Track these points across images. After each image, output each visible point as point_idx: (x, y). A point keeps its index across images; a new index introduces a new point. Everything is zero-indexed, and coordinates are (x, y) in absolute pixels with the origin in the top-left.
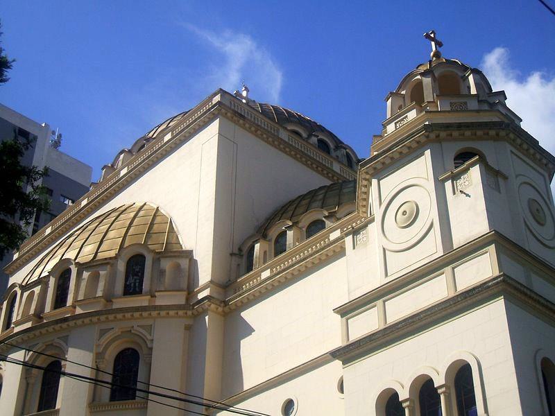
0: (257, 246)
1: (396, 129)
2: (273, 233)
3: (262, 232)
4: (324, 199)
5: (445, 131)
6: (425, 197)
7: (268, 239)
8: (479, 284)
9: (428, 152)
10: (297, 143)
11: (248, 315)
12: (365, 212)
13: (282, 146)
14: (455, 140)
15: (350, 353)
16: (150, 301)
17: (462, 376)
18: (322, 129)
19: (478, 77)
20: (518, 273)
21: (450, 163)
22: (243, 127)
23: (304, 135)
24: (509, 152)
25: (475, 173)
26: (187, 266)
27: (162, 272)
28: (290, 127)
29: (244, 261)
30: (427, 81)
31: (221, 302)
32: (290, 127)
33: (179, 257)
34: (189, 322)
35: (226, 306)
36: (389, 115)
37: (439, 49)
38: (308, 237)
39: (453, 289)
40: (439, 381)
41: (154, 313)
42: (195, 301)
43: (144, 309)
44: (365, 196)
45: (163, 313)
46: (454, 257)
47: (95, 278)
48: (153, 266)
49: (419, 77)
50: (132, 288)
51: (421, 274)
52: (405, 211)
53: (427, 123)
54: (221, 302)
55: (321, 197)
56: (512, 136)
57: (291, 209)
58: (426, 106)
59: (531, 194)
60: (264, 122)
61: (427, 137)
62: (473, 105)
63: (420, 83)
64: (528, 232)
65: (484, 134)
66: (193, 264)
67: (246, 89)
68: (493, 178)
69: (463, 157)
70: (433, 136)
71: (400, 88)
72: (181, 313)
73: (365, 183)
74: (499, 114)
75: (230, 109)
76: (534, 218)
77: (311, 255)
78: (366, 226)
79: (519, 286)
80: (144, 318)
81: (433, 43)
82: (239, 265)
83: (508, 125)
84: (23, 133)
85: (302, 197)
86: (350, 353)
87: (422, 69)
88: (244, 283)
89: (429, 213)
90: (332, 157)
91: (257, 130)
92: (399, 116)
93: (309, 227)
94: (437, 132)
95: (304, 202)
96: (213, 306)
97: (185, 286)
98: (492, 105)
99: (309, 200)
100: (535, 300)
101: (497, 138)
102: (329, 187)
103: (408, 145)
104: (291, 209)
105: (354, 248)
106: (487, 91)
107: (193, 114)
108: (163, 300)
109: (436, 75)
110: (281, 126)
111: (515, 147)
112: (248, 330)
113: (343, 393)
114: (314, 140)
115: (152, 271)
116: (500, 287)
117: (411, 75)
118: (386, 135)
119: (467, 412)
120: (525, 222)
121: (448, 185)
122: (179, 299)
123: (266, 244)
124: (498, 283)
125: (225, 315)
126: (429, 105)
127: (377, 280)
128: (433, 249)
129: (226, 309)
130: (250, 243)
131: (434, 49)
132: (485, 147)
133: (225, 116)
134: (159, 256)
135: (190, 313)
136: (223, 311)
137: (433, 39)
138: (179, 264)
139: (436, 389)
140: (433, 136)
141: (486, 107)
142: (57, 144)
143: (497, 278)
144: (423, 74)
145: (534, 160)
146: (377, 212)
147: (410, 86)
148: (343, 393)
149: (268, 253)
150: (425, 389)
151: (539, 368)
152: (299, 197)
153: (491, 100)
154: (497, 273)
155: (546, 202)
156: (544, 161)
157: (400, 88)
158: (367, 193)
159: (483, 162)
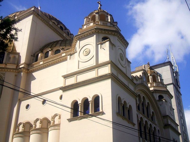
0: (40, 54)
1: (87, 27)
2: (45, 51)
3: (41, 50)
4: (61, 44)
5: (100, 30)
7: (43, 53)
8: (104, 74)
9: (95, 36)
10: (54, 26)
11: (34, 74)
12: (74, 50)
13: (54, 30)
14: (103, 33)
15: (65, 89)
16: (5, 66)
17: (96, 99)
18: (62, 23)
19: (111, 17)
20: (115, 73)
21: (101, 40)
22: (39, 19)
23: (56, 24)
24: (117, 40)
25: (107, 44)
26: (18, 57)
27: (10, 58)
28: (53, 21)
29: (35, 58)
30: (97, 15)
31: (27, 69)
32: (53, 21)
33: (15, 54)
34: (16, 74)
35: (28, 70)
36: (85, 23)
37: (101, 7)
38: (55, 54)
39: (97, 75)
40: (90, 99)
41: (6, 70)
42: (19, 68)
43: (3, 68)
44: (75, 45)
45: (9, 70)
46: (99, 66)
48: (7, 56)
49: (95, 14)
51: (89, 69)
52: (86, 51)
53: (96, 27)
54: (27, 69)
55: (60, 43)
56: (118, 35)
57: (51, 45)
58: (96, 22)
59: (120, 51)
60: (45, 18)
61: (95, 31)
62: (109, 24)
63: (95, 16)
64: (119, 63)
65: (111, 33)
66: (20, 57)
67: (40, 7)
68: (112, 45)
69: (105, 39)
70: (97, 31)
71: (89, 16)
72: (14, 71)
73: (75, 41)
74: (115, 28)
75: (37, 13)
76: (121, 59)
77: (56, 59)
78: (74, 54)
79: (115, 77)
80: (3, 71)
81: (99, 5)
82: (33, 59)
83: (118, 32)
85: (54, 42)
86: (65, 89)
87: (96, 12)
88: (34, 64)
89: (93, 53)
90: (63, 32)
91: (43, 20)
92: (88, 24)
93: (56, 51)
94: (98, 30)
95: (55, 44)
96: (24, 70)
97: (16, 63)
98: (114, 25)
99: (56, 43)
100: (120, 82)
101: (114, 35)
102: (62, 40)
103: (90, 33)
104: (51, 45)
105: (70, 59)
106: (113, 21)
107: (25, 12)
108: (9, 66)
109: (100, 14)
110: (50, 20)
111: (119, 38)
112: (34, 78)
114: (59, 26)
115: (7, 57)
116: (110, 76)
117: (92, 13)
118: (83, 29)
119: (96, 109)
120: (119, 60)
121: (99, 46)
122: (14, 67)
123: (42, 54)
124: (110, 75)
125: (27, 73)
126: (97, 22)
127: (76, 70)
128: (93, 63)
129: (28, 72)
130: (38, 53)
131: (99, 6)
132: (111, 37)
133: (35, 14)
135: (17, 71)
136: (27, 72)
137: (100, 4)
138: (15, 57)
139: (89, 102)
140: (97, 31)
141: (112, 26)
143: (110, 73)
144: (96, 13)
145: (123, 43)
146: (78, 50)
147: (92, 16)
149: (42, 57)
150: (86, 102)
151: (117, 99)
152: (53, 42)
153: (114, 24)
154: (110, 72)
155: (124, 54)
156: (125, 43)
157: (89, 16)
158: (75, 44)
159: (110, 41)
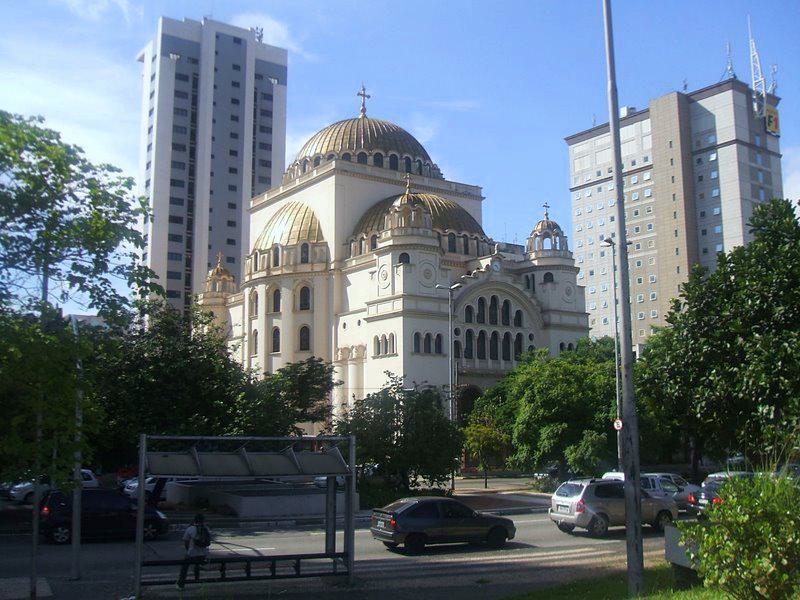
6: (388, 269)
27: (315, 254)
47: (289, 254)
50: (305, 261)
84: (237, 41)
113: (648, 110)
128: (388, 293)
134: (314, 245)
142: (260, 37)
148: (648, 110)
